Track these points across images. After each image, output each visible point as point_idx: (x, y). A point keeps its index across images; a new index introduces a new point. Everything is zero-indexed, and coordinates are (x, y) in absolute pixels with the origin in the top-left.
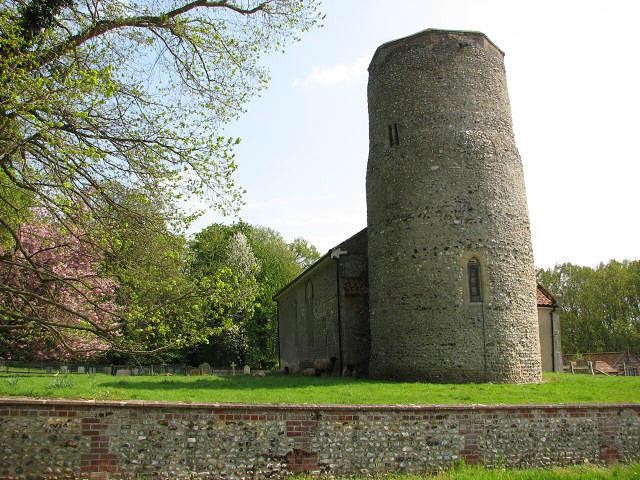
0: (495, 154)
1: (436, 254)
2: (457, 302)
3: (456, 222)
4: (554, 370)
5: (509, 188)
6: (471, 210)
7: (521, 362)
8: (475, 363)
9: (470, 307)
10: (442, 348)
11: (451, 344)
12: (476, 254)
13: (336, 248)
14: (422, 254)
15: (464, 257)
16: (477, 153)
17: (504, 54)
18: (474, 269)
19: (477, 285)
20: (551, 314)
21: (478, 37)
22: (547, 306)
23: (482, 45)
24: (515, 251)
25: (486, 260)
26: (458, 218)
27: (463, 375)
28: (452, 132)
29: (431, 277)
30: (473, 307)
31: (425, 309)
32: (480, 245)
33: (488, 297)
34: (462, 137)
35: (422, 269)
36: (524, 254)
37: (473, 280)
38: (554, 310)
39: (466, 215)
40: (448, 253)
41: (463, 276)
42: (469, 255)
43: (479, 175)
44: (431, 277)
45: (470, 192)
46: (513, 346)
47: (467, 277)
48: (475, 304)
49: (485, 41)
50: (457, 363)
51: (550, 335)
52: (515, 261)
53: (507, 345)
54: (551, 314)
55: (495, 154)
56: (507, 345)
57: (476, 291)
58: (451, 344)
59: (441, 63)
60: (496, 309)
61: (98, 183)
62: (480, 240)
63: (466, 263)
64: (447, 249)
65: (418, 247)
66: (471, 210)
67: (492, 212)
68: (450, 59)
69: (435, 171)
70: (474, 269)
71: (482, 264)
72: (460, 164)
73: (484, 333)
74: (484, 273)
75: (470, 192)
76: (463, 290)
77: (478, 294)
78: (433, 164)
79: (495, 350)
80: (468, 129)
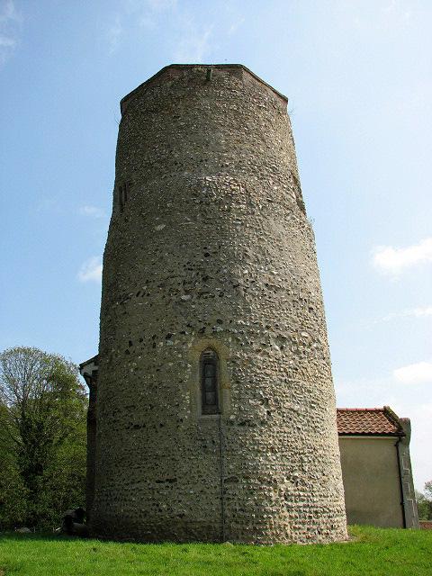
0: (250, 204)
1: (154, 347)
2: (180, 416)
3: (184, 297)
4: (405, 527)
5: (274, 252)
6: (206, 279)
7: (289, 509)
8: (206, 511)
9: (201, 422)
10: (157, 486)
11: (170, 481)
12: (214, 342)
13: (89, 362)
14: (137, 347)
15: (194, 348)
16: (220, 203)
17: (286, 100)
18: (209, 364)
19: (214, 388)
20: (397, 446)
21: (236, 70)
22: (390, 434)
23: (241, 79)
24: (281, 339)
25: (228, 350)
26: (187, 292)
27: (186, 530)
28: (185, 180)
29: (146, 379)
30: (206, 421)
31: (137, 427)
32: (220, 328)
33: (230, 407)
34: (199, 184)
35: (136, 369)
36: (308, 344)
37: (209, 382)
38: (400, 440)
39: (199, 287)
40: (170, 342)
41: (191, 376)
42: (203, 343)
43: (222, 233)
44: (146, 379)
45: (207, 255)
46: (273, 483)
47: (198, 377)
48: (207, 416)
49: (245, 73)
50: (177, 510)
51: (396, 475)
52: (280, 353)
53: (262, 481)
54: (397, 446)
55: (250, 204)
56: (262, 481)
57: (211, 402)
58: (170, 481)
59: (178, 99)
60: (243, 424)
61: (207, 398)
62: (220, 322)
63: (197, 355)
64: (169, 337)
65: (134, 338)
66: (206, 279)
67: (241, 281)
68: (191, 94)
69: (160, 232)
70: (209, 364)
71: (222, 357)
72: (194, 219)
73: (220, 462)
74: (225, 370)
75: (207, 255)
76: (190, 396)
77: (216, 401)
78: (159, 224)
79: (238, 489)
80: (210, 174)
